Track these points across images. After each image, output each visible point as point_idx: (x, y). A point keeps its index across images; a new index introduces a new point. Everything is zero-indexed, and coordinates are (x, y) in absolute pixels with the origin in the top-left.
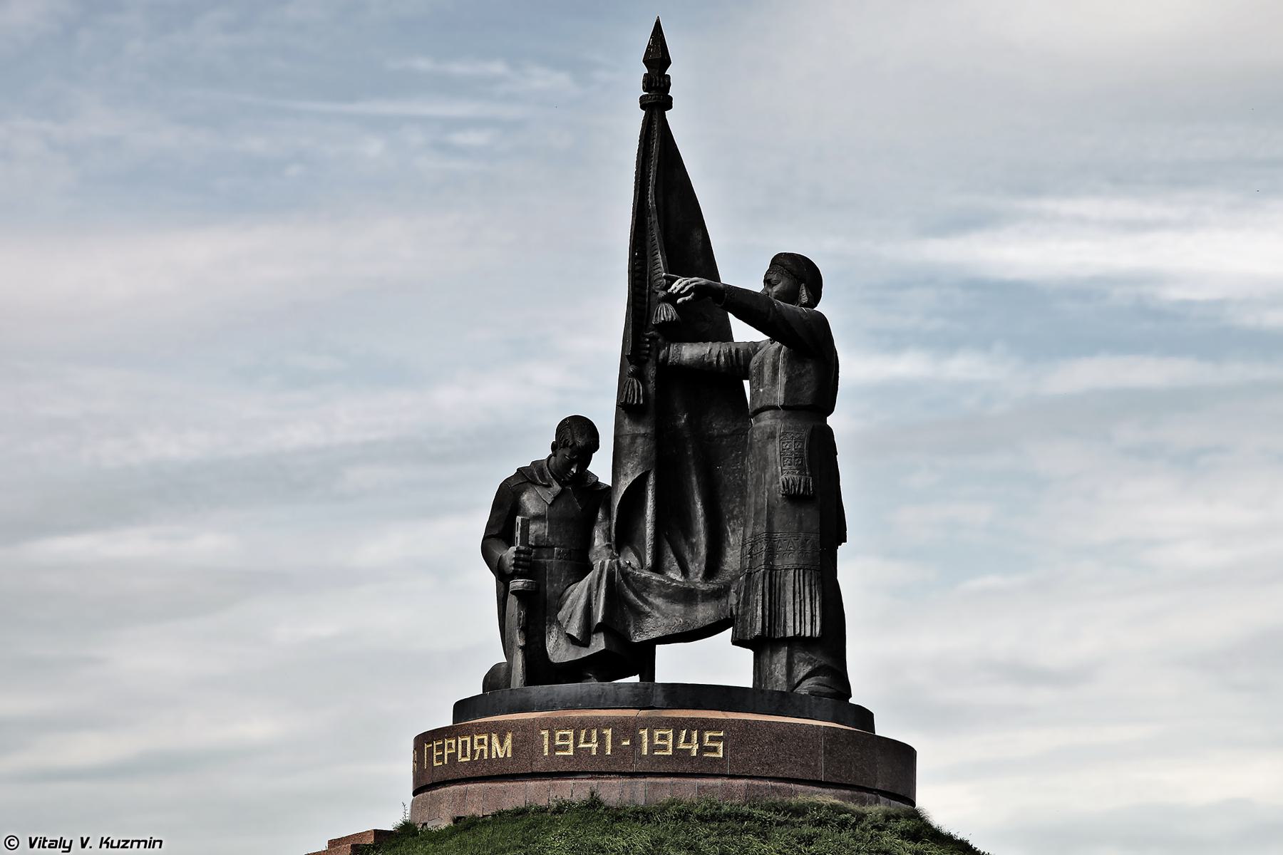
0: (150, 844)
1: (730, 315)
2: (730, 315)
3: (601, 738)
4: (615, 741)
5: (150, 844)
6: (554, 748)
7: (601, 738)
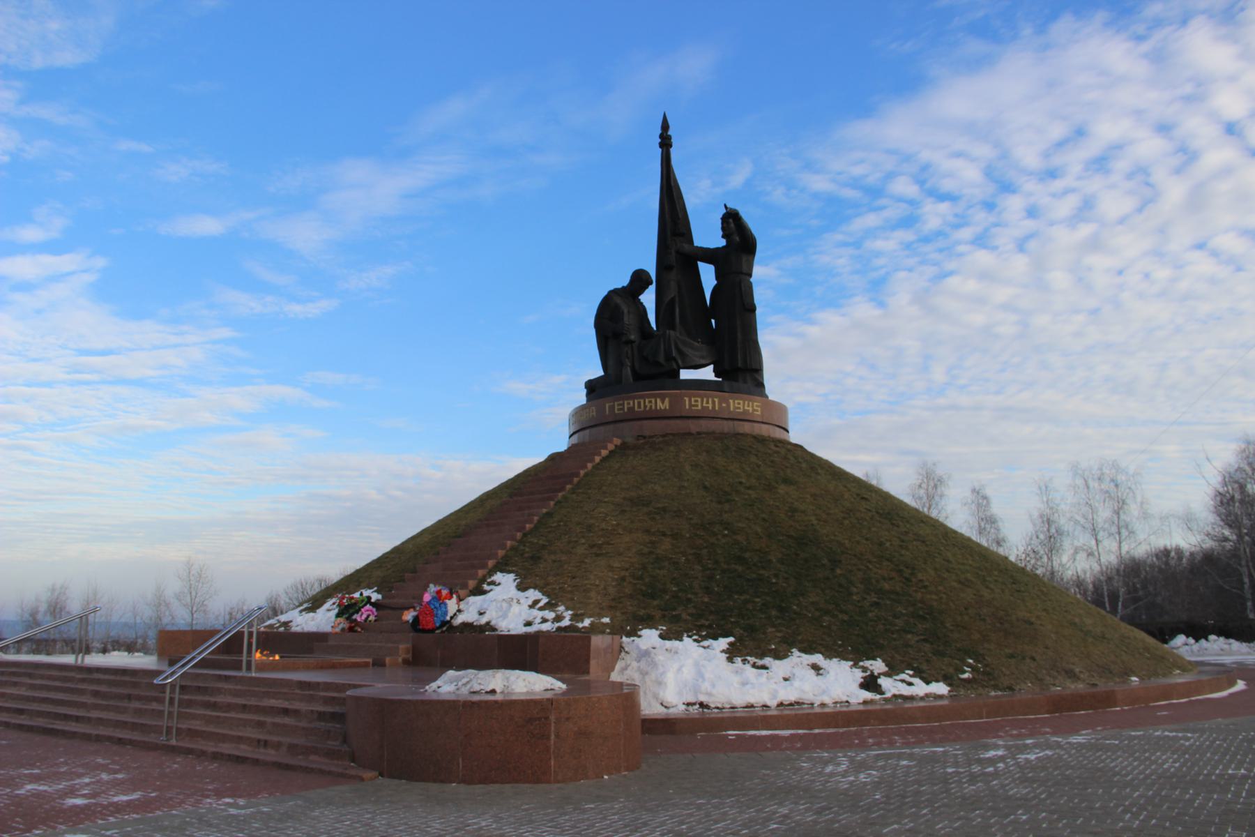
0: (666, 143)
1: (700, 264)
2: (700, 264)
3: (714, 403)
4: (720, 403)
5: (666, 143)
6: (691, 405)
7: (714, 403)
